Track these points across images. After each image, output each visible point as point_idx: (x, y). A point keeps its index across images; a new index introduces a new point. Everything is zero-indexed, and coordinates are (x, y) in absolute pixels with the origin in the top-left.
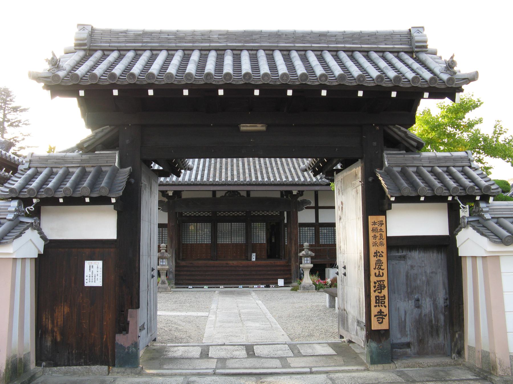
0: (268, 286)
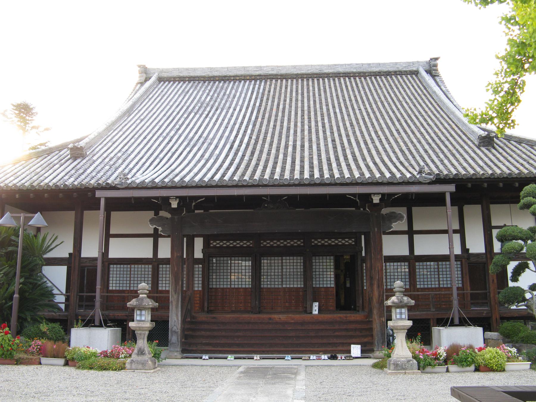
0: (333, 357)
